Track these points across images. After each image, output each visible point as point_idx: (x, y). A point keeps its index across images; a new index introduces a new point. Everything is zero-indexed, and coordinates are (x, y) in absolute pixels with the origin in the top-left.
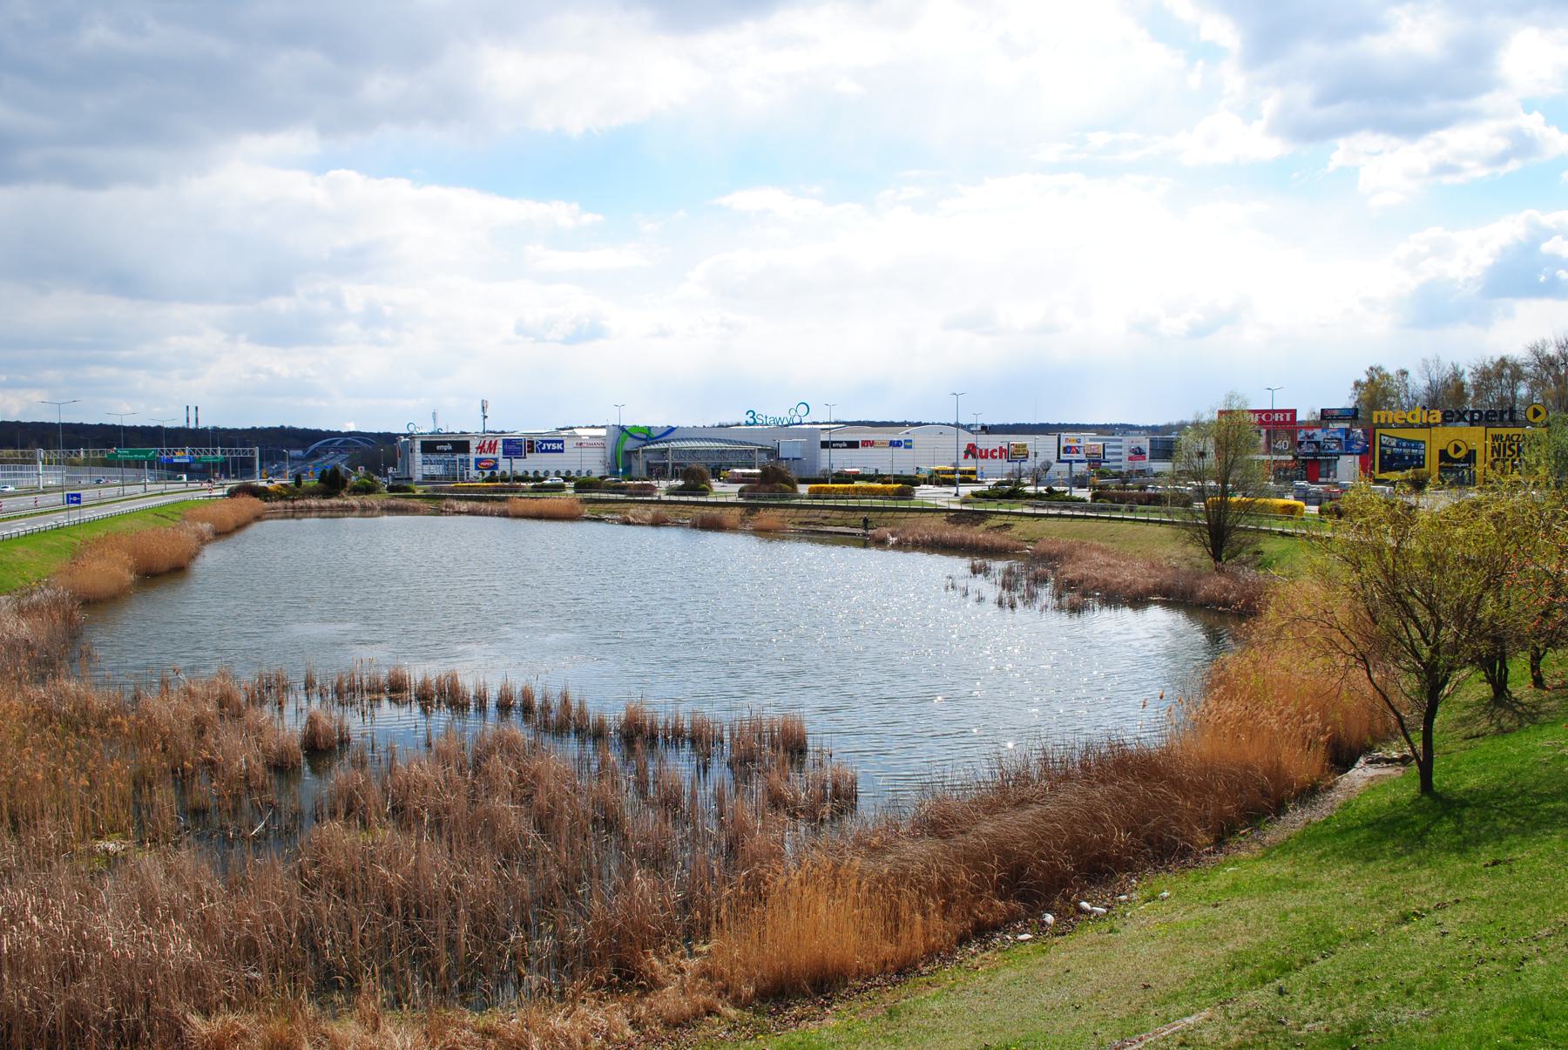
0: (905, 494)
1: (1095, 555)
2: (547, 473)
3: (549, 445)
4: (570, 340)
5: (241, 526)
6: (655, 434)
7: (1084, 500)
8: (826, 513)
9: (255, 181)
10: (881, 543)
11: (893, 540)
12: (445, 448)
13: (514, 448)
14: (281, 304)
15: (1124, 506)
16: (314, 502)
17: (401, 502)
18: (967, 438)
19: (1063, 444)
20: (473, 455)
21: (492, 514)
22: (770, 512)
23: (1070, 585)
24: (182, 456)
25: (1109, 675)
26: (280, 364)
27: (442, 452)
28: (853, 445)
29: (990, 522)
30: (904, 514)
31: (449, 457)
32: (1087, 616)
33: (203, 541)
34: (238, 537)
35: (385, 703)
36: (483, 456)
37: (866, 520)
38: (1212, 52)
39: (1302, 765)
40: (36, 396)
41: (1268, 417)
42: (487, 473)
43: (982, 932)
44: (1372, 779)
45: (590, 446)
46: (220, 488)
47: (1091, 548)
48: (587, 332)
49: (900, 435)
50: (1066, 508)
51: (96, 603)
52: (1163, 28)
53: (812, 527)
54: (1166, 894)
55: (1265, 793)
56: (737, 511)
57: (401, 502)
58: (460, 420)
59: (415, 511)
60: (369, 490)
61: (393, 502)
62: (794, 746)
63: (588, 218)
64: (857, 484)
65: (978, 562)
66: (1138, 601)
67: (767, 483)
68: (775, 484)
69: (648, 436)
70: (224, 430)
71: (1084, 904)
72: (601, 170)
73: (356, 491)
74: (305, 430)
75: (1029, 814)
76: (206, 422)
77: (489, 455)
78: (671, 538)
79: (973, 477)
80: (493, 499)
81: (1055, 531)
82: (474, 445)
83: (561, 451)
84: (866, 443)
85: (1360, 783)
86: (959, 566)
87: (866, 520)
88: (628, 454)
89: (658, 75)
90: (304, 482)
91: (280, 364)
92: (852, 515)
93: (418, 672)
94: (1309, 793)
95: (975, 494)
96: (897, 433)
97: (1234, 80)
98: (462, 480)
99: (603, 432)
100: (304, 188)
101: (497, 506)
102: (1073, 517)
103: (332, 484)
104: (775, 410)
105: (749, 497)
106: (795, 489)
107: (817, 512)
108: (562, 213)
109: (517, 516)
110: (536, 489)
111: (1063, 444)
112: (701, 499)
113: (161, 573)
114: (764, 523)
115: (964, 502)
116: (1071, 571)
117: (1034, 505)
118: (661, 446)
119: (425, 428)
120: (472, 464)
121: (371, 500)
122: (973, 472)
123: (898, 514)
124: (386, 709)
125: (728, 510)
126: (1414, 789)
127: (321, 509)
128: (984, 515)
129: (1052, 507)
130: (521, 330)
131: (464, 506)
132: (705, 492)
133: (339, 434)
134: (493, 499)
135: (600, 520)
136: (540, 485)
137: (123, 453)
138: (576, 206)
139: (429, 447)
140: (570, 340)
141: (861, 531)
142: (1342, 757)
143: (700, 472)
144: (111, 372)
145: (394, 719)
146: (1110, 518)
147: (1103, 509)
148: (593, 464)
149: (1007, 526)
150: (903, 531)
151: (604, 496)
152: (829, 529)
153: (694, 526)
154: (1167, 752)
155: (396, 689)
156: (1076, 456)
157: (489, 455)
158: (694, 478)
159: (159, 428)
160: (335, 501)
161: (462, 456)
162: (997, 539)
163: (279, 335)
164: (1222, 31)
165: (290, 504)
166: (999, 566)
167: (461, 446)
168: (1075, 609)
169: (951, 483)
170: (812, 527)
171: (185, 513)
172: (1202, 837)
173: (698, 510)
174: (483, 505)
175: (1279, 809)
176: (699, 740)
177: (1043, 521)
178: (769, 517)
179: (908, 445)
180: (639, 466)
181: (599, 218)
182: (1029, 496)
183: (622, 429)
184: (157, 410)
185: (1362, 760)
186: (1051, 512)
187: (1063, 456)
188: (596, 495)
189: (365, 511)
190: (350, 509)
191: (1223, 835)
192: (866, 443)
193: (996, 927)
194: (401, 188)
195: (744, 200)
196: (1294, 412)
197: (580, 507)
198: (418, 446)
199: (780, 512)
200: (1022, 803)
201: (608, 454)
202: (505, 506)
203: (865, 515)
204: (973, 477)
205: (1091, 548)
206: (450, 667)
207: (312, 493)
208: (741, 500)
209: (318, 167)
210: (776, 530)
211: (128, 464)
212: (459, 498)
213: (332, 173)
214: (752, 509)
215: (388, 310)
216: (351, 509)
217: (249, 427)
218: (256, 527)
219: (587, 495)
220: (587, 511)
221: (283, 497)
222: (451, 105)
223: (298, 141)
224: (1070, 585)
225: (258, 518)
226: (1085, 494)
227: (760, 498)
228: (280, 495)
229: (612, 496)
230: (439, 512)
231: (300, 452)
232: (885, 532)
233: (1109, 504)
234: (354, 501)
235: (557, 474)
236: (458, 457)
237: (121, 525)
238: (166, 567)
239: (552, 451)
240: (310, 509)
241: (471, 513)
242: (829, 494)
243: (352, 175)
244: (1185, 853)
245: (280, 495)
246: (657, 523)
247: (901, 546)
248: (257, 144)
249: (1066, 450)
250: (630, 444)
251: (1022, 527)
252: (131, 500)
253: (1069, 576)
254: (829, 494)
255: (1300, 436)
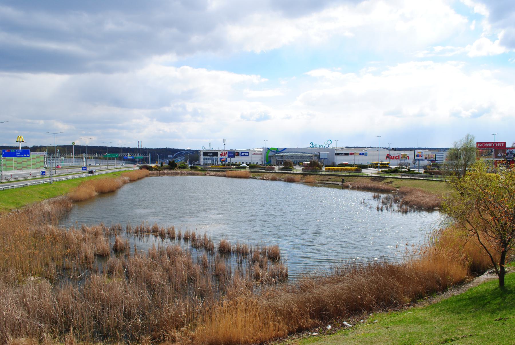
0: (358, 171)
1: (419, 192)
2: (243, 163)
3: (244, 154)
4: (258, 120)
5: (139, 179)
6: (279, 150)
7: (421, 173)
8: (330, 177)
9: (159, 70)
10: (347, 187)
11: (351, 186)
12: (210, 154)
13: (231, 154)
14: (167, 109)
15: (434, 176)
16: (166, 171)
17: (194, 172)
18: (387, 152)
19: (416, 154)
20: (219, 157)
21: (221, 176)
22: (311, 176)
23: (406, 203)
24: (129, 157)
25: (409, 235)
26: (166, 128)
27: (209, 156)
28: (347, 154)
29: (386, 181)
30: (356, 178)
31: (211, 158)
32: (409, 214)
33: (125, 183)
34: (139, 181)
35: (151, 236)
36: (222, 157)
37: (343, 180)
38: (478, 17)
39: (457, 271)
40: (94, 138)
41: (484, 145)
42: (224, 163)
43: (301, 330)
44: (488, 279)
45: (257, 154)
46: (137, 166)
47: (417, 190)
48: (264, 117)
49: (363, 151)
50: (413, 176)
51: (77, 201)
52: (460, 9)
53: (324, 182)
54: (376, 321)
55: (438, 282)
56: (300, 176)
57: (194, 172)
58: (217, 147)
59: (197, 175)
60: (184, 168)
61: (191, 172)
62: (274, 257)
63: (263, 80)
64: (346, 167)
65: (376, 194)
66: (430, 209)
67: (311, 167)
68: (316, 167)
69: (277, 151)
70: (149, 149)
71: (345, 323)
72: (266, 64)
73: (180, 168)
74: (173, 149)
75: (340, 285)
76: (144, 147)
77: (224, 157)
78: (280, 185)
79: (387, 166)
80: (222, 171)
81: (407, 184)
82: (219, 153)
83: (248, 156)
84: (351, 154)
85: (483, 280)
86: (369, 195)
87: (343, 180)
88: (270, 157)
89: (285, 32)
90: (164, 165)
91: (166, 128)
92: (338, 178)
93: (165, 226)
94: (460, 283)
95: (382, 171)
96: (362, 151)
97: (486, 25)
98: (216, 165)
99: (262, 150)
100: (173, 72)
101: (223, 173)
102: (415, 179)
103: (172, 166)
104: (320, 142)
105: (305, 171)
106: (321, 169)
107: (326, 177)
108: (255, 79)
109: (229, 177)
110: (237, 168)
111: (416, 154)
112: (291, 172)
113: (106, 192)
114: (308, 180)
115: (378, 174)
116: (407, 198)
117: (397, 176)
118: (281, 154)
119: (207, 148)
120: (219, 160)
121: (184, 171)
122: (388, 164)
123: (354, 178)
124: (152, 238)
125: (297, 175)
126: (497, 285)
127: (168, 174)
128: (384, 178)
129: (408, 176)
130: (243, 117)
131: (212, 173)
132: (291, 169)
133: (184, 150)
134: (222, 171)
135: (255, 178)
136: (238, 167)
137: (108, 155)
138: (259, 76)
139: (205, 154)
140: (258, 120)
141: (341, 183)
142: (476, 270)
143: (290, 163)
144: (116, 131)
145: (152, 243)
146: (428, 180)
147: (426, 177)
148: (257, 160)
149: (391, 182)
150: (355, 183)
151: (257, 170)
152: (330, 182)
153: (285, 181)
154: (405, 266)
155: (155, 232)
156: (421, 158)
157: (224, 157)
158: (288, 166)
159: (129, 148)
160: (173, 171)
161: (216, 157)
162: (386, 187)
163: (166, 119)
164: (482, 10)
165: (158, 172)
166: (383, 196)
167: (215, 154)
168: (405, 212)
169: (377, 167)
170: (324, 182)
171: (123, 174)
172: (407, 299)
173: (287, 176)
174: (218, 173)
175: (444, 289)
176: (243, 253)
177: (404, 181)
178: (310, 178)
179: (366, 154)
180: (273, 161)
181: (267, 80)
182: (401, 172)
183: (268, 148)
184: (129, 142)
185: (487, 272)
186: (407, 177)
187: (416, 158)
188: (254, 170)
189: (182, 174)
190: (177, 174)
191: (417, 298)
192: (351, 154)
193: (307, 329)
194: (203, 71)
195: (315, 73)
196: (505, 143)
197: (249, 174)
198: (202, 154)
199: (314, 176)
200: (339, 282)
201: (263, 156)
202: (225, 173)
203: (343, 178)
204: (387, 166)
205: (417, 190)
206: (172, 224)
207: (166, 168)
208: (302, 172)
209: (178, 65)
210: (312, 183)
211: (110, 159)
212: (212, 171)
213: (182, 67)
214: (305, 175)
215: (200, 111)
216: (178, 173)
217: (156, 148)
218: (147, 179)
219: (252, 170)
220: (251, 175)
221: (156, 170)
222: (217, 45)
223: (171, 57)
224: (406, 203)
225: (147, 176)
226: (422, 171)
227: (308, 171)
228: (155, 169)
229: (260, 170)
230: (205, 175)
231: (171, 156)
232: (348, 184)
233: (429, 175)
234: (179, 171)
235: (246, 163)
236: (214, 157)
237: (100, 177)
238: (108, 191)
239: (245, 156)
240: (165, 173)
241: (215, 175)
242: (332, 170)
243: (188, 68)
244: (396, 305)
245: (155, 169)
246: (273, 179)
247: (353, 188)
248: (157, 59)
249: (417, 156)
250: (271, 154)
251: (396, 182)
252: (106, 170)
253: (406, 200)
254: (332, 170)
255: (507, 152)
